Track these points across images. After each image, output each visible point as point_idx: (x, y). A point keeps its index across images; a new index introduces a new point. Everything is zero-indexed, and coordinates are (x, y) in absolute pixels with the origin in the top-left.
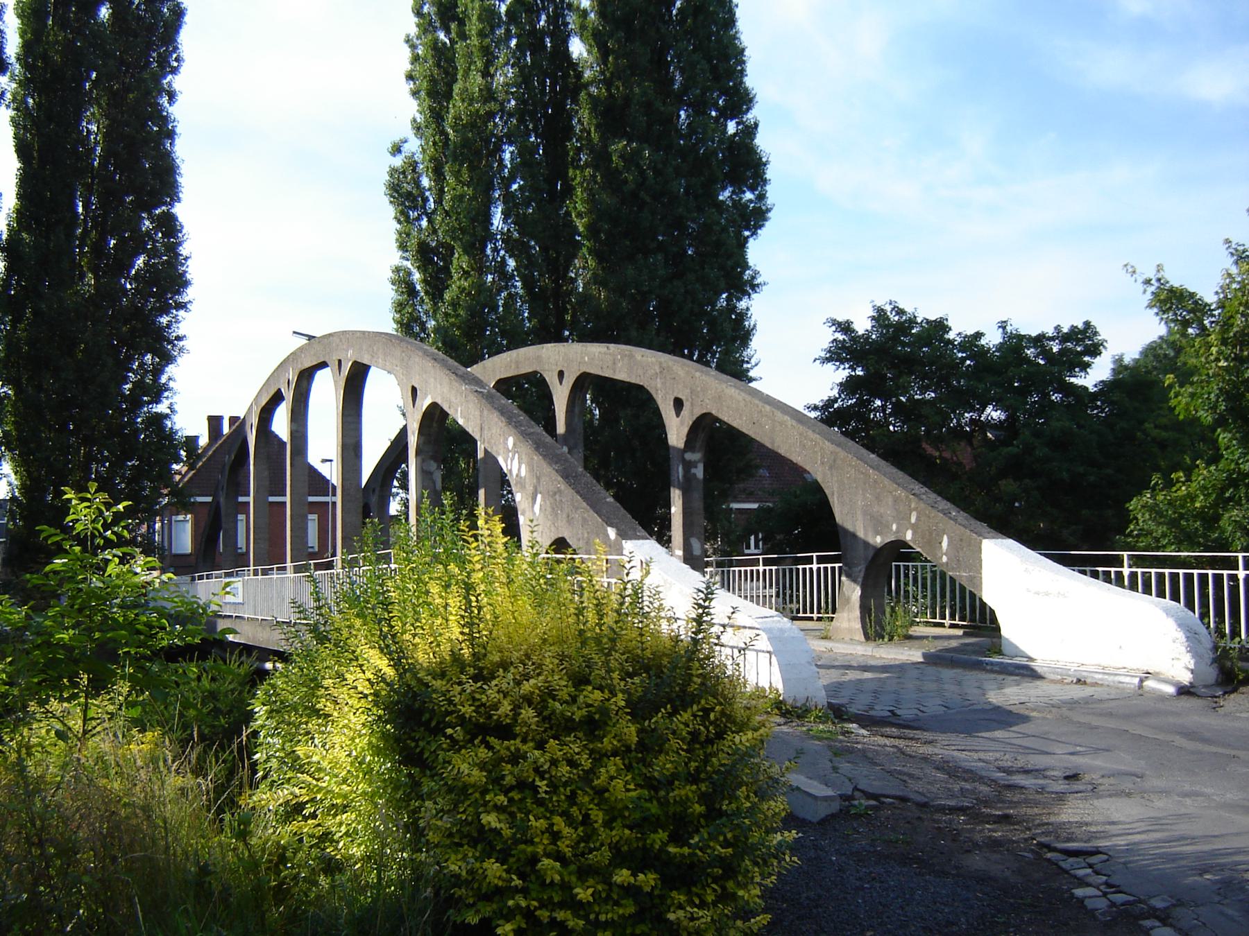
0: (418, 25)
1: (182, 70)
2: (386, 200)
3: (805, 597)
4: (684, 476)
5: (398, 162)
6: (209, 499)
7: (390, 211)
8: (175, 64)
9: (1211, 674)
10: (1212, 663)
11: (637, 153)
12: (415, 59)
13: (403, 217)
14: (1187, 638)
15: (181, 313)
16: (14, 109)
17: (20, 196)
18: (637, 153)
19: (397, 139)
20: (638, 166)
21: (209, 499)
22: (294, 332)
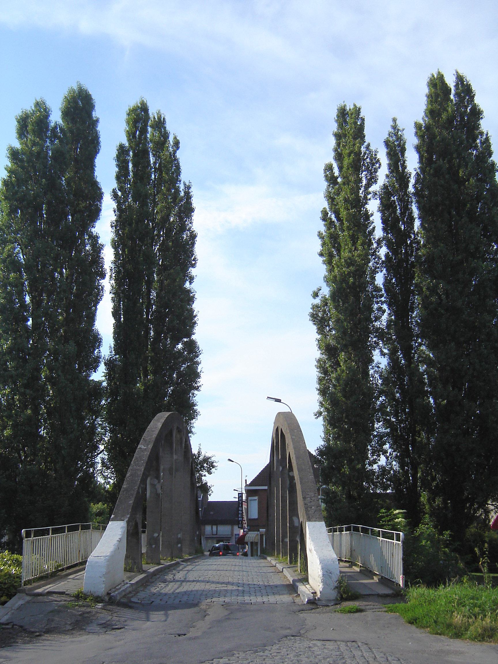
0: (325, 225)
1: (197, 265)
2: (311, 323)
3: (390, 544)
4: (290, 484)
5: (318, 301)
6: (266, 488)
7: (314, 328)
8: (194, 262)
9: (333, 594)
10: (334, 589)
11: (436, 286)
12: (323, 245)
13: (321, 330)
14: (323, 575)
15: (196, 392)
16: (113, 294)
17: (116, 339)
18: (436, 286)
19: (315, 289)
20: (437, 294)
21: (266, 488)
22: (268, 397)
